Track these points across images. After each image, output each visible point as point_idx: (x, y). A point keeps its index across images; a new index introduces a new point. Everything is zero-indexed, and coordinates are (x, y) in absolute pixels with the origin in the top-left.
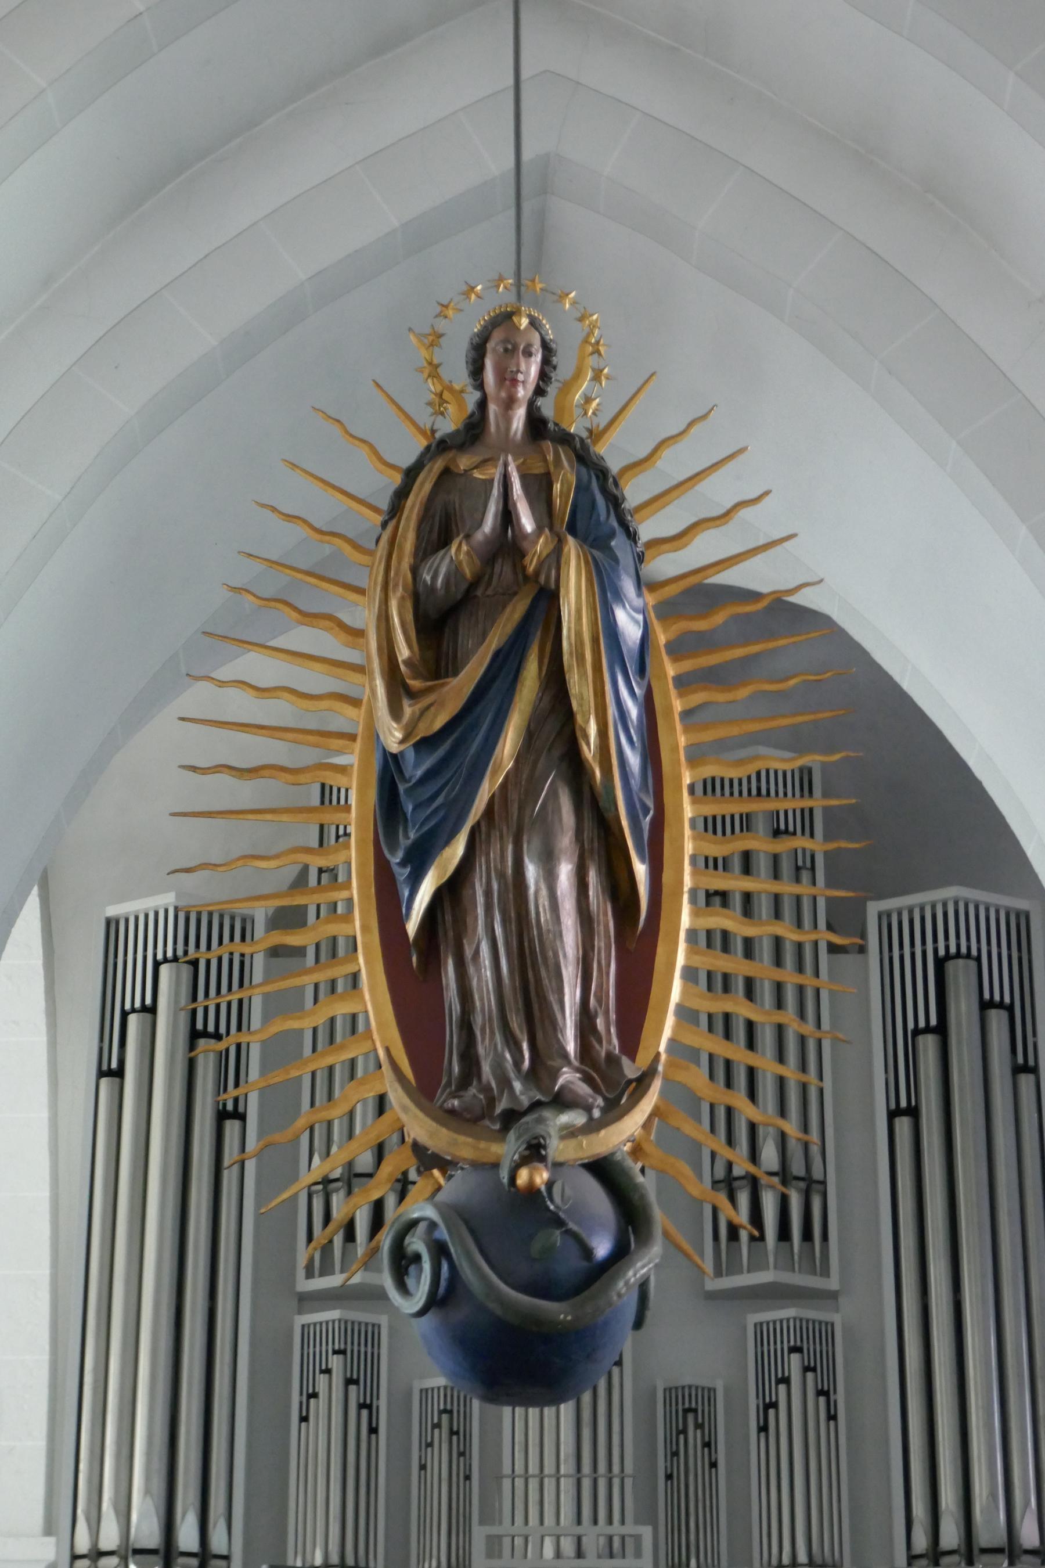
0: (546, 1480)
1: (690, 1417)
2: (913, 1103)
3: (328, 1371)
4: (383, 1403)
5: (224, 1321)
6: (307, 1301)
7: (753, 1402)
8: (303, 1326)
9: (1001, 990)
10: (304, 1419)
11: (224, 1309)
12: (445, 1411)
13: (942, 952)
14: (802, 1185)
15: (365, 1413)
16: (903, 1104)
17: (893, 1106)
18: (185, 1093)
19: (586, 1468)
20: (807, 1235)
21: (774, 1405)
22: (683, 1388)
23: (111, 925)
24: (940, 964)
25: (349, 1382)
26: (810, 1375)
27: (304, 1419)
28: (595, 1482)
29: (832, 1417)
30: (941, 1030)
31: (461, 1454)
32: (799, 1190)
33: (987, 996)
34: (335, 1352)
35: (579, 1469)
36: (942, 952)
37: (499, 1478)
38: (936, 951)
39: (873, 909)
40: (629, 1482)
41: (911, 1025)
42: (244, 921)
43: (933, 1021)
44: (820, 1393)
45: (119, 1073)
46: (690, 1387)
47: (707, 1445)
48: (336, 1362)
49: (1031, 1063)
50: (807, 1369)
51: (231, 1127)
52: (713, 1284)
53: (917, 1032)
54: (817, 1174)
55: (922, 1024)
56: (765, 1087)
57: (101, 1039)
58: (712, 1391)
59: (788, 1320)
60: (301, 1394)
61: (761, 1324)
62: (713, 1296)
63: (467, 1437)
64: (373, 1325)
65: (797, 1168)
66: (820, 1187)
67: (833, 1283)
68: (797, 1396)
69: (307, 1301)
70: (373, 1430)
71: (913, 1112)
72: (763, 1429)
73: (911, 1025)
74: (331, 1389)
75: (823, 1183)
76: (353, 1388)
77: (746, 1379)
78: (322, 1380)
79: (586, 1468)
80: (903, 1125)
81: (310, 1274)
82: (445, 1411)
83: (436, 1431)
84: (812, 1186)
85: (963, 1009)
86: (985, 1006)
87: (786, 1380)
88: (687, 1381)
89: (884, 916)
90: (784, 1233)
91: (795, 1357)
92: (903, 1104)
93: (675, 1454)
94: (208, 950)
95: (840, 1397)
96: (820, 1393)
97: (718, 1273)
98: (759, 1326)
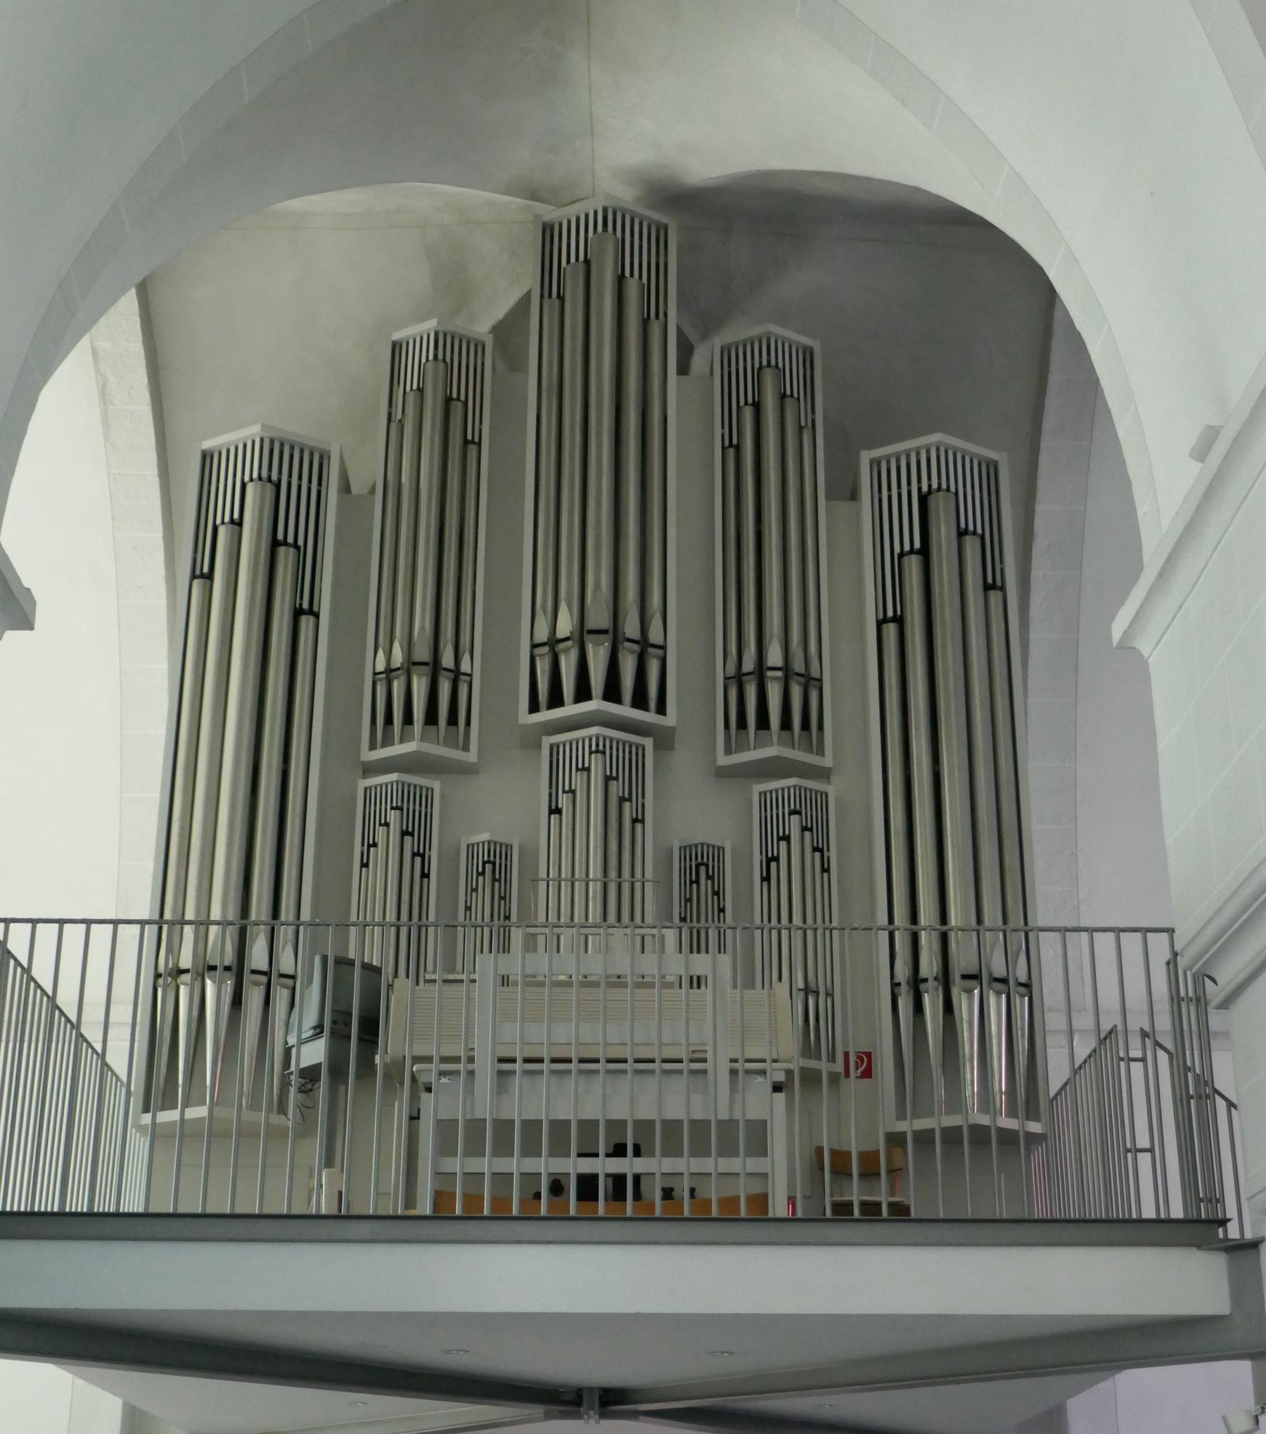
0: (577, 884)
1: (703, 869)
2: (899, 612)
3: (387, 824)
4: (434, 855)
5: (296, 780)
6: (370, 769)
7: (757, 857)
8: (366, 789)
9: (976, 521)
10: (365, 865)
11: (293, 823)
12: (489, 862)
13: (925, 489)
14: (802, 679)
15: (418, 860)
16: (890, 613)
17: (881, 617)
18: (261, 651)
19: (613, 874)
20: (806, 725)
21: (777, 859)
22: (696, 846)
23: (206, 457)
24: (923, 499)
25: (404, 833)
26: (807, 834)
27: (365, 865)
28: (619, 886)
29: (825, 870)
30: (924, 552)
31: (502, 898)
32: (799, 683)
33: (963, 525)
34: (392, 808)
35: (605, 874)
36: (925, 489)
37: (536, 880)
38: (920, 489)
39: (866, 457)
40: (649, 887)
41: (897, 549)
42: (321, 457)
43: (917, 545)
44: (815, 849)
45: (210, 576)
46: (702, 845)
47: (716, 893)
48: (393, 817)
49: (999, 583)
50: (804, 829)
51: (306, 622)
52: (723, 760)
53: (902, 555)
54: (815, 673)
55: (907, 548)
56: (771, 581)
57: (195, 551)
58: (721, 849)
59: (789, 789)
60: (363, 845)
61: (765, 793)
62: (725, 773)
63: (508, 882)
64: (427, 789)
65: (798, 666)
66: (817, 683)
67: (828, 761)
68: (797, 850)
69: (370, 769)
70: (425, 875)
71: (899, 620)
72: (766, 879)
73: (897, 549)
74: (388, 839)
75: (820, 680)
76: (408, 839)
77: (751, 842)
78: (381, 831)
79: (613, 874)
80: (891, 630)
81: (373, 746)
82: (489, 862)
83: (481, 878)
84: (811, 682)
85: (943, 533)
86: (962, 533)
87: (787, 838)
88: (700, 839)
89: (876, 463)
90: (786, 724)
91: (795, 818)
92: (890, 613)
93: (689, 900)
94: (292, 473)
95: (833, 854)
96: (815, 849)
97: (728, 751)
98: (763, 794)
